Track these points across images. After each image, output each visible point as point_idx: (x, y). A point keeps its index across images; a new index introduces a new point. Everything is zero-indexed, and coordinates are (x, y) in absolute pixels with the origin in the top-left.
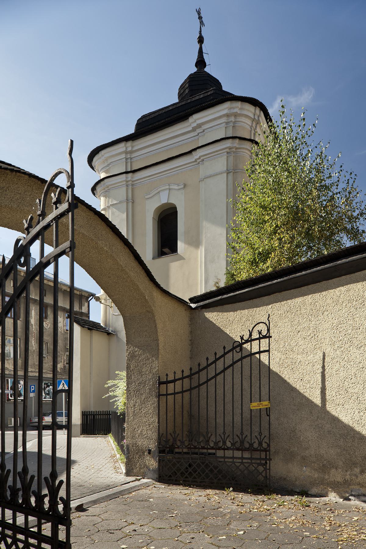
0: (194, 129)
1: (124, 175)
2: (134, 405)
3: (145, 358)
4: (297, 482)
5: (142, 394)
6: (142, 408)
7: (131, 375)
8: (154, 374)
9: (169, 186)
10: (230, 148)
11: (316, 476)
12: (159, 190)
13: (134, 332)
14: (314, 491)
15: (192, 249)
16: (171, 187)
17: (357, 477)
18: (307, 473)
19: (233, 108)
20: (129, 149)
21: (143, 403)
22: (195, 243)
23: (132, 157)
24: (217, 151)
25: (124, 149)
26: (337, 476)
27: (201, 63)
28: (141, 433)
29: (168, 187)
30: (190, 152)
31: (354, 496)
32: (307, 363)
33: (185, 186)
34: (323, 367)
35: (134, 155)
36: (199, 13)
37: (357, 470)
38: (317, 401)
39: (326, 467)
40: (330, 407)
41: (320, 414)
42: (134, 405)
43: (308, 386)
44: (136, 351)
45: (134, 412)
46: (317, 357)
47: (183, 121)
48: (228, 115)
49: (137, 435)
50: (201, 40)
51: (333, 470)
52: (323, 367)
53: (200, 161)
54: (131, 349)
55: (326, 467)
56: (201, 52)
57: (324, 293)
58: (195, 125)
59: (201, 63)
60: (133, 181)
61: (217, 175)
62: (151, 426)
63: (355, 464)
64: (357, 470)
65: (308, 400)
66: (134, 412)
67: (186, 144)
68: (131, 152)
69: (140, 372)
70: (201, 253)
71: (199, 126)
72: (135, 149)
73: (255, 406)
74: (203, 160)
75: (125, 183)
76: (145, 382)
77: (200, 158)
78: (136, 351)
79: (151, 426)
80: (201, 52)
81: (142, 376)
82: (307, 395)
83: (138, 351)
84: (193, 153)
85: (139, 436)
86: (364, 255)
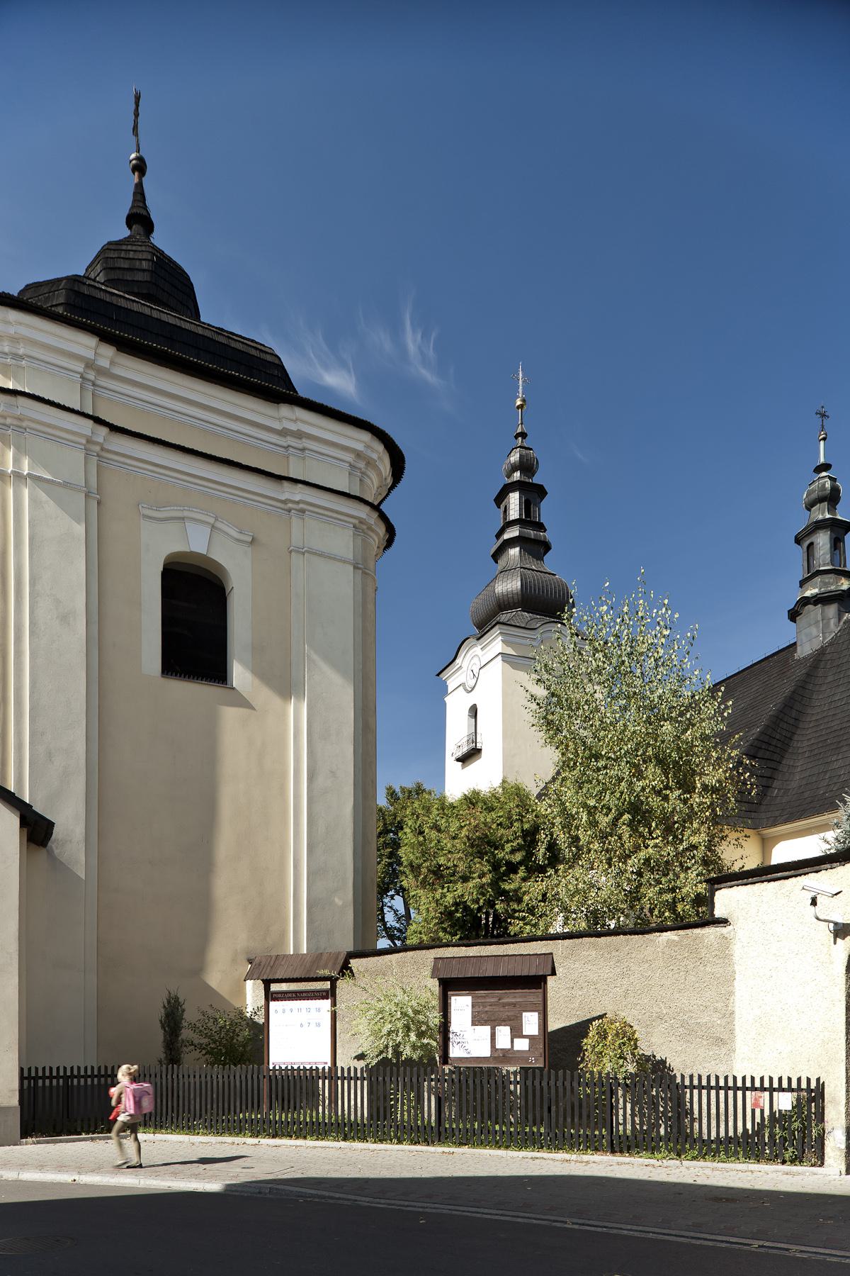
0: (284, 433)
1: (90, 422)
9: (216, 520)
10: (362, 521)
12: (186, 514)
15: (276, 701)
16: (219, 525)
19: (373, 450)
20: (104, 363)
22: (286, 686)
23: (98, 382)
24: (337, 512)
25: (90, 354)
27: (140, 219)
29: (212, 520)
30: (114, 429)
33: (253, 541)
35: (103, 382)
36: (138, 98)
47: (182, 372)
48: (358, 455)
50: (140, 167)
53: (288, 508)
56: (139, 192)
58: (293, 427)
59: (140, 219)
60: (102, 449)
61: (334, 559)
67: (244, 443)
68: (101, 372)
70: (296, 714)
71: (299, 435)
72: (117, 371)
74: (303, 511)
75: (84, 441)
77: (298, 503)
80: (139, 192)
84: (286, 484)
86: (10, 1175)
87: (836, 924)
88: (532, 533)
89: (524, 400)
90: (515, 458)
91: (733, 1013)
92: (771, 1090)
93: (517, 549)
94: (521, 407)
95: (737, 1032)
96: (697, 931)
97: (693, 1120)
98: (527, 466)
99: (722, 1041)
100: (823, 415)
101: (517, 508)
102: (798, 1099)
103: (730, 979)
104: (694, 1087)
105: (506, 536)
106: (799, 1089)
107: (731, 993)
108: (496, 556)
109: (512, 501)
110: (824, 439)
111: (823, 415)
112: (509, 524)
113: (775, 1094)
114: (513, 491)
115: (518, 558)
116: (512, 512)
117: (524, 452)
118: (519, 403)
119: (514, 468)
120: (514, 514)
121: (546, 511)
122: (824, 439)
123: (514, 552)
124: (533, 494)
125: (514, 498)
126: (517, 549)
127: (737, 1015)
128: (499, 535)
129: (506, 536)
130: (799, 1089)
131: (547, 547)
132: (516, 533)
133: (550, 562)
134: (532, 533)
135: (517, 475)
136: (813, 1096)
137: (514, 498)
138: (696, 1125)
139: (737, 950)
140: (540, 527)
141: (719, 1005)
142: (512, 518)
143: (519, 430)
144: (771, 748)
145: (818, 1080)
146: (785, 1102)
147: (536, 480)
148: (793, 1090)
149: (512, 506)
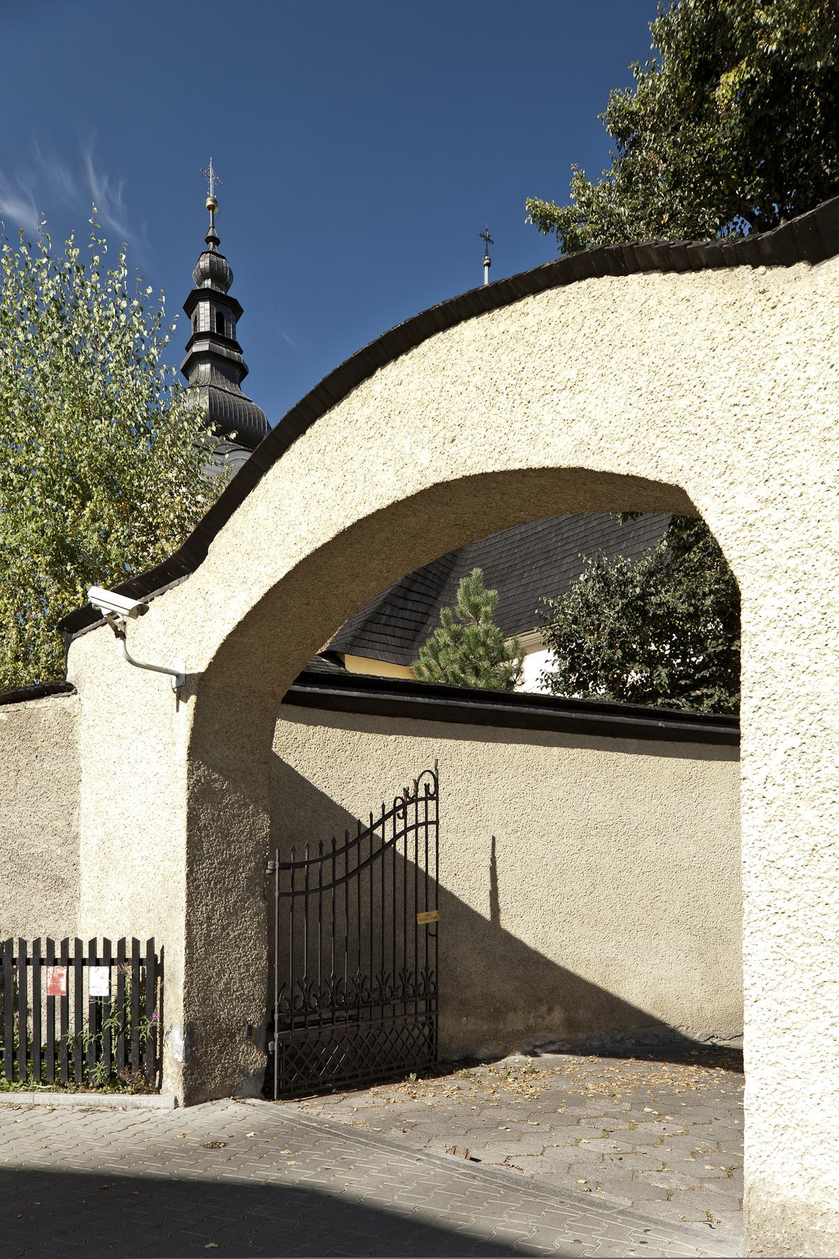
2: (209, 918)
3: (237, 802)
4: (454, 1045)
5: (229, 891)
6: (229, 924)
7: (200, 841)
8: (258, 843)
11: (485, 1028)
13: (217, 732)
14: (483, 1052)
17: (543, 1018)
18: (470, 1026)
21: (233, 914)
26: (515, 1022)
28: (227, 989)
31: (540, 1047)
32: (464, 848)
34: (493, 860)
37: (544, 1009)
38: (484, 910)
39: (499, 1010)
40: (507, 923)
41: (489, 934)
42: (209, 918)
43: (467, 885)
44: (216, 780)
45: (208, 935)
46: (480, 840)
49: (216, 995)
51: (511, 1014)
52: (493, 860)
54: (200, 772)
55: (499, 1010)
57: (491, 745)
62: (252, 969)
63: (540, 1001)
64: (544, 1009)
65: (466, 907)
66: (208, 935)
69: (225, 835)
73: (423, 918)
76: (239, 859)
78: (216, 780)
79: (252, 969)
81: (229, 843)
82: (464, 900)
83: (221, 785)
85: (221, 996)
87: (178, 676)
88: (225, 351)
89: (215, 201)
90: (204, 263)
91: (76, 837)
92: (80, 963)
93: (208, 366)
94: (211, 208)
95: (83, 868)
96: (31, 704)
97: (25, 1013)
98: (218, 274)
99: (61, 883)
100: (488, 239)
101: (208, 320)
102: (121, 978)
103: (74, 783)
104: (28, 962)
105: (195, 349)
106: (122, 959)
107: (75, 804)
108: (187, 370)
109: (202, 311)
110: (488, 265)
111: (488, 239)
112: (199, 336)
113: (85, 969)
114: (204, 300)
115: (208, 376)
116: (202, 324)
117: (215, 258)
118: (209, 202)
119: (205, 275)
120: (205, 325)
121: (242, 331)
122: (488, 265)
123: (205, 368)
124: (227, 309)
125: (204, 308)
126: (208, 366)
127: (82, 841)
128: (188, 348)
129: (195, 349)
130: (122, 959)
131: (243, 371)
132: (206, 348)
133: (247, 388)
134: (225, 351)
135: (208, 283)
136: (143, 969)
137: (204, 308)
138: (30, 1021)
139: (84, 735)
140: (234, 346)
141: (60, 824)
142: (202, 330)
143: (210, 234)
144: (428, 583)
145: (151, 943)
146: (98, 982)
147: (231, 293)
148: (111, 962)
149: (202, 317)
